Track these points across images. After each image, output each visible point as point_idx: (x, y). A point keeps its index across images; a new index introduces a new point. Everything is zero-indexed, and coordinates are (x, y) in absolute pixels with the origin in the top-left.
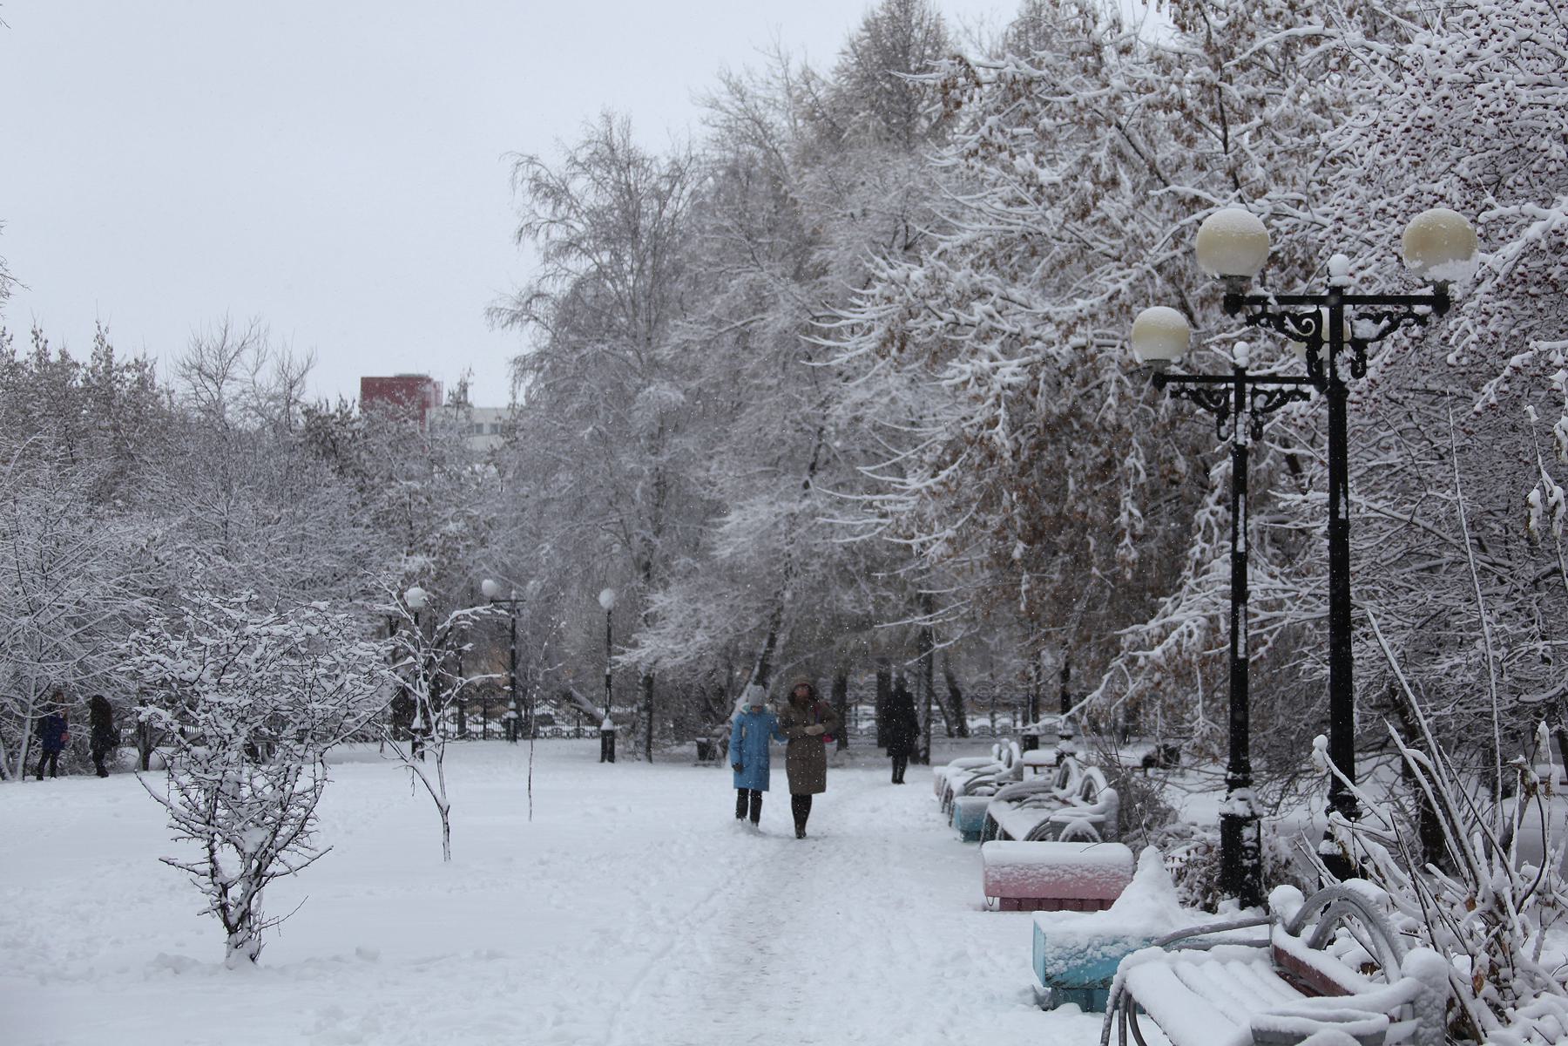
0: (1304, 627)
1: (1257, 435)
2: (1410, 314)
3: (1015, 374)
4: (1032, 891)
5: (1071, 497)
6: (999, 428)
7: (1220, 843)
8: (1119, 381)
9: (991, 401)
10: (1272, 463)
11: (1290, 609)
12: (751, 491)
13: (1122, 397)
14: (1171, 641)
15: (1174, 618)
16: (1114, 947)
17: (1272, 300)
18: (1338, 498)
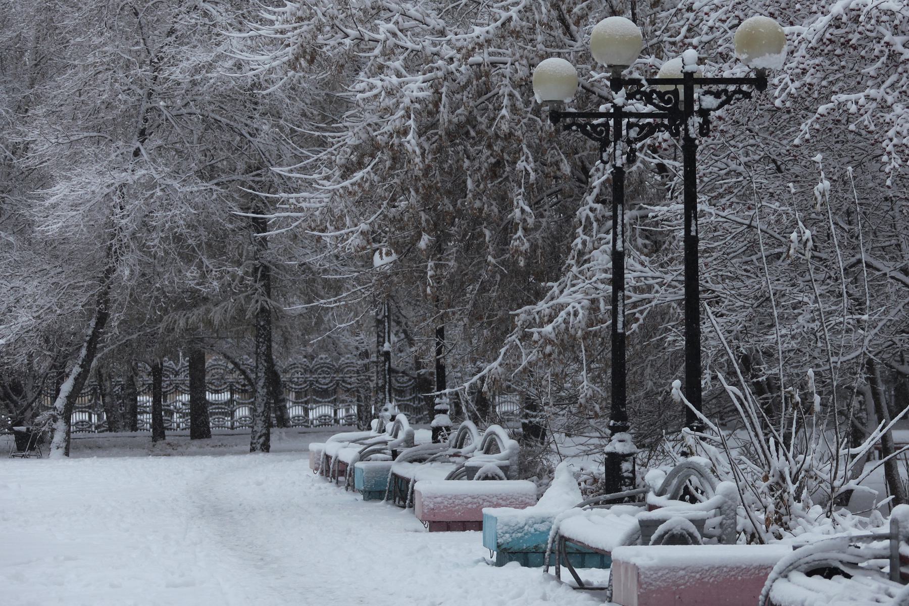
0: (669, 306)
2: (739, 91)
3: (421, 89)
4: (458, 516)
5: (470, 195)
6: (410, 137)
7: (604, 476)
8: (511, 95)
9: (402, 112)
10: (642, 166)
11: (657, 292)
12: (75, 159)
13: (514, 109)
14: (559, 319)
15: (562, 300)
16: (542, 525)
17: (644, 82)
18: (691, 221)
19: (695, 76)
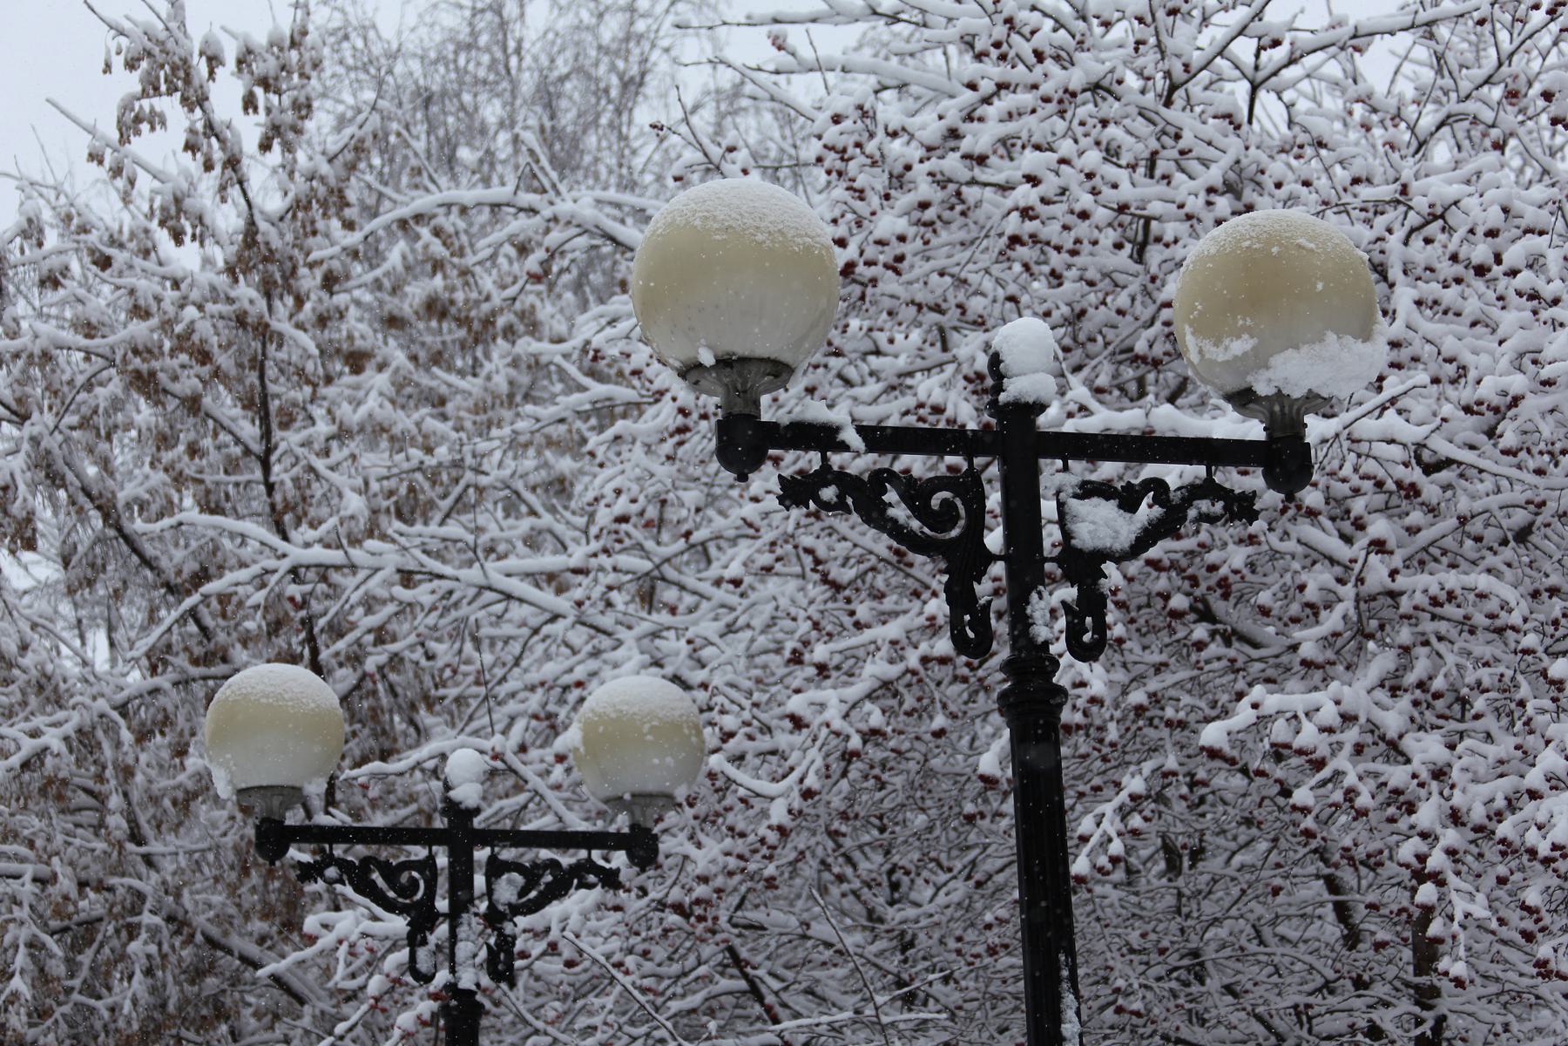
1: (501, 965)
13: (42, 977)
19: (1047, 421)
